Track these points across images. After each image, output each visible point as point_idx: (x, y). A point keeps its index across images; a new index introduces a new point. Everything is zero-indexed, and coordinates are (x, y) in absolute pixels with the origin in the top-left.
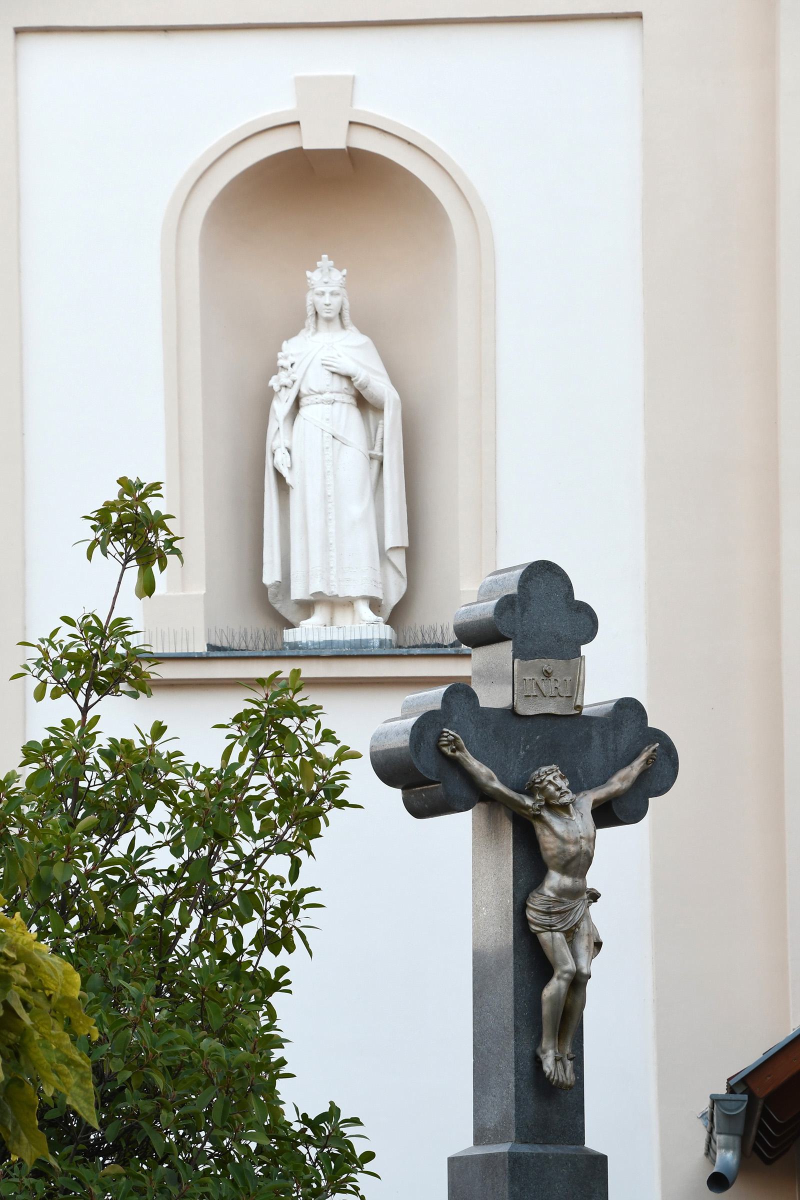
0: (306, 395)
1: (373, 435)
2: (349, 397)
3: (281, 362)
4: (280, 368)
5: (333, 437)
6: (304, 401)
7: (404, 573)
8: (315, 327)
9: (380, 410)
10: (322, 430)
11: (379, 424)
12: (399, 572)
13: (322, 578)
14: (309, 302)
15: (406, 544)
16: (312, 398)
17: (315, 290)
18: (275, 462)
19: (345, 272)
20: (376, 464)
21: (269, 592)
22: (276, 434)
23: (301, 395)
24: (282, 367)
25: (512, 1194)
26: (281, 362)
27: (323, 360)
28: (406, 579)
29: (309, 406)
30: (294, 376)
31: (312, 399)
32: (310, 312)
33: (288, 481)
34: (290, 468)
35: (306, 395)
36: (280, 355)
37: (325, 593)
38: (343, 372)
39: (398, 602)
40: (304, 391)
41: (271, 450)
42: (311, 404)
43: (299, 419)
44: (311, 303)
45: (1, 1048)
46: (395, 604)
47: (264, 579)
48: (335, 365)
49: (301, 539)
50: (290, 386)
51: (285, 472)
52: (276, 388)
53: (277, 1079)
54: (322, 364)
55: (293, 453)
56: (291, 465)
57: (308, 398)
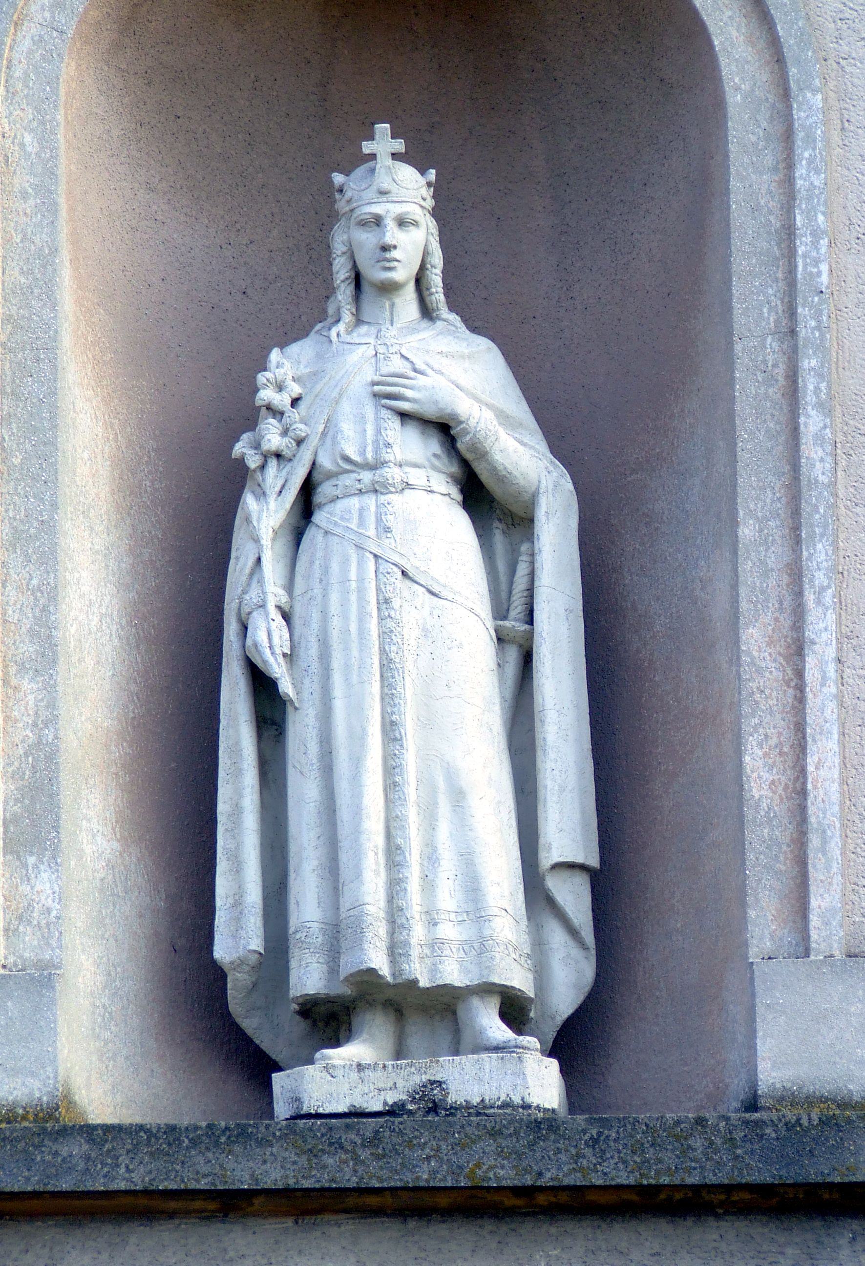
0: (330, 476)
1: (504, 587)
2: (443, 478)
3: (266, 395)
4: (264, 409)
5: (404, 573)
6: (324, 491)
7: (589, 938)
8: (354, 310)
9: (522, 519)
10: (376, 556)
11: (519, 554)
12: (573, 932)
13: (331, 1128)
14: (339, 246)
15: (594, 861)
16: (347, 480)
17: (357, 212)
18: (249, 642)
19: (432, 174)
20: (513, 655)
21: (229, 986)
22: (251, 575)
23: (316, 476)
24: (269, 408)
25: (11, 1117)
26: (266, 395)
27: (378, 384)
28: (594, 952)
29: (338, 501)
30: (301, 429)
31: (348, 482)
32: (341, 271)
33: (286, 687)
34: (290, 657)
35: (330, 476)
36: (261, 378)
37: (381, 973)
38: (430, 411)
39: (573, 1014)
40: (326, 462)
41: (239, 614)
42: (345, 496)
43: (311, 534)
44: (344, 249)
45: (543, 1265)
46: (565, 1016)
47: (216, 948)
48: (409, 393)
49: (319, 837)
50: (287, 453)
51: (278, 669)
52: (253, 462)
53: (257, 373)
54: (375, 395)
55: (297, 621)
56: (292, 647)
57: (334, 481)
